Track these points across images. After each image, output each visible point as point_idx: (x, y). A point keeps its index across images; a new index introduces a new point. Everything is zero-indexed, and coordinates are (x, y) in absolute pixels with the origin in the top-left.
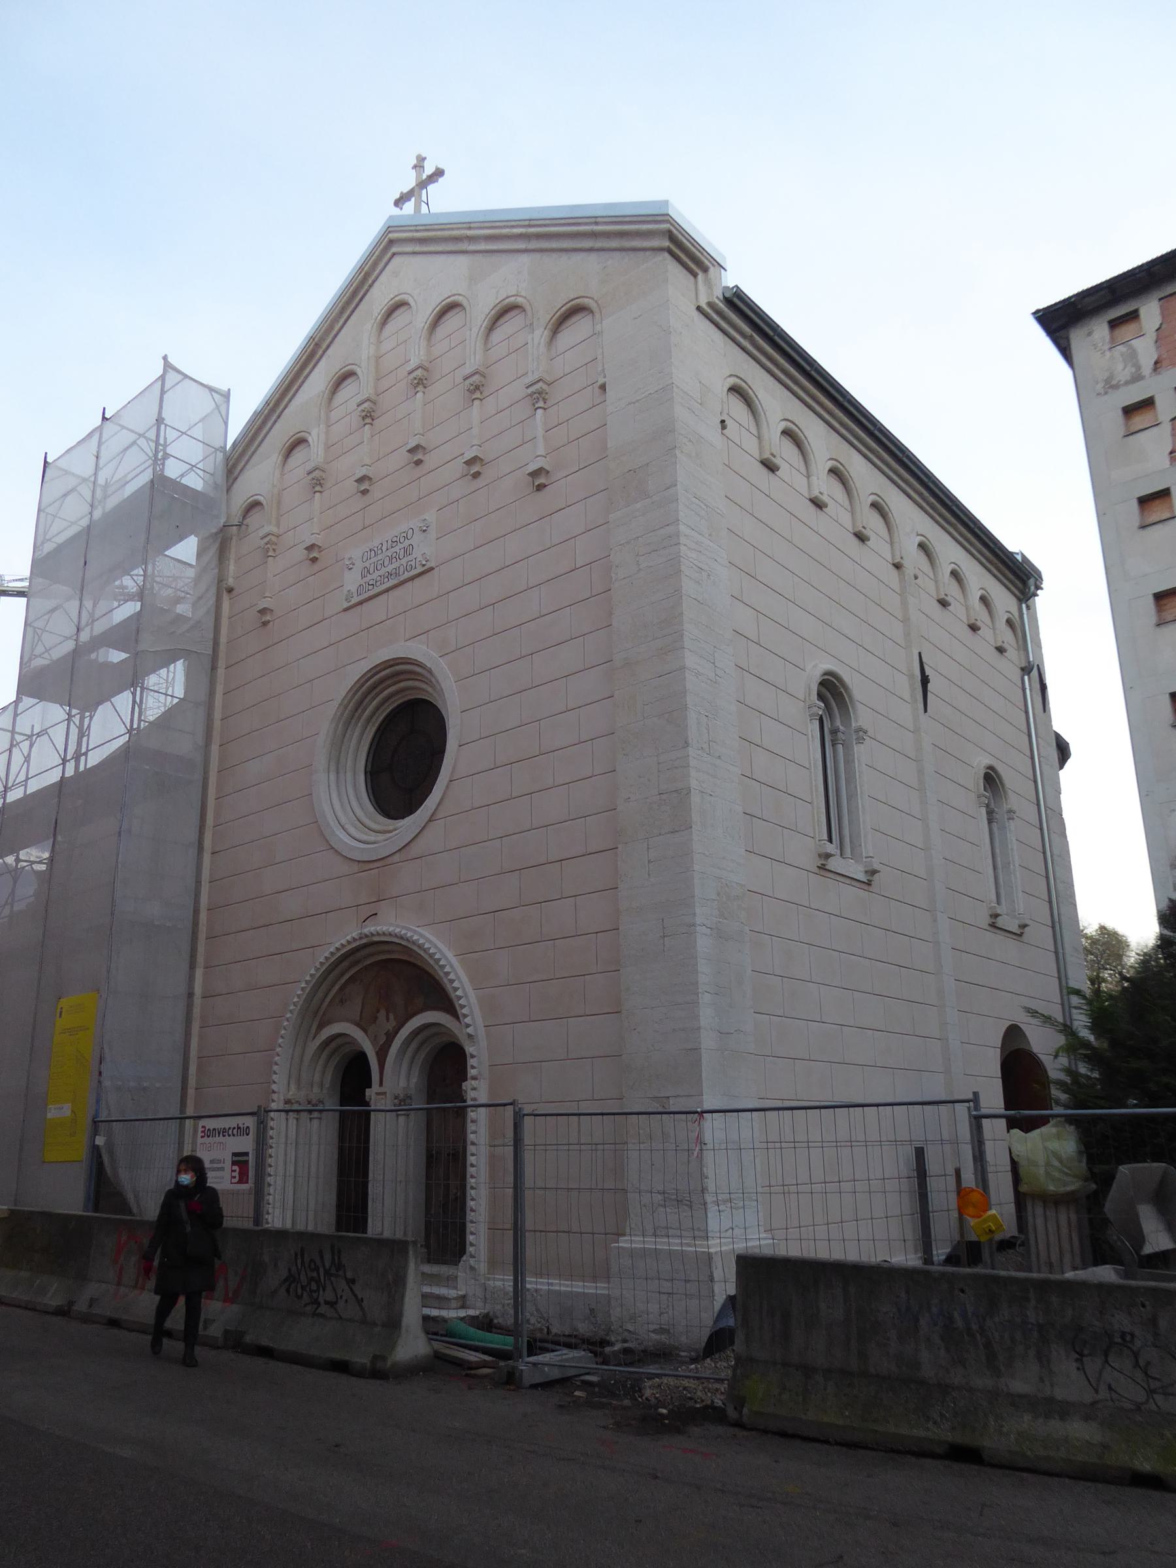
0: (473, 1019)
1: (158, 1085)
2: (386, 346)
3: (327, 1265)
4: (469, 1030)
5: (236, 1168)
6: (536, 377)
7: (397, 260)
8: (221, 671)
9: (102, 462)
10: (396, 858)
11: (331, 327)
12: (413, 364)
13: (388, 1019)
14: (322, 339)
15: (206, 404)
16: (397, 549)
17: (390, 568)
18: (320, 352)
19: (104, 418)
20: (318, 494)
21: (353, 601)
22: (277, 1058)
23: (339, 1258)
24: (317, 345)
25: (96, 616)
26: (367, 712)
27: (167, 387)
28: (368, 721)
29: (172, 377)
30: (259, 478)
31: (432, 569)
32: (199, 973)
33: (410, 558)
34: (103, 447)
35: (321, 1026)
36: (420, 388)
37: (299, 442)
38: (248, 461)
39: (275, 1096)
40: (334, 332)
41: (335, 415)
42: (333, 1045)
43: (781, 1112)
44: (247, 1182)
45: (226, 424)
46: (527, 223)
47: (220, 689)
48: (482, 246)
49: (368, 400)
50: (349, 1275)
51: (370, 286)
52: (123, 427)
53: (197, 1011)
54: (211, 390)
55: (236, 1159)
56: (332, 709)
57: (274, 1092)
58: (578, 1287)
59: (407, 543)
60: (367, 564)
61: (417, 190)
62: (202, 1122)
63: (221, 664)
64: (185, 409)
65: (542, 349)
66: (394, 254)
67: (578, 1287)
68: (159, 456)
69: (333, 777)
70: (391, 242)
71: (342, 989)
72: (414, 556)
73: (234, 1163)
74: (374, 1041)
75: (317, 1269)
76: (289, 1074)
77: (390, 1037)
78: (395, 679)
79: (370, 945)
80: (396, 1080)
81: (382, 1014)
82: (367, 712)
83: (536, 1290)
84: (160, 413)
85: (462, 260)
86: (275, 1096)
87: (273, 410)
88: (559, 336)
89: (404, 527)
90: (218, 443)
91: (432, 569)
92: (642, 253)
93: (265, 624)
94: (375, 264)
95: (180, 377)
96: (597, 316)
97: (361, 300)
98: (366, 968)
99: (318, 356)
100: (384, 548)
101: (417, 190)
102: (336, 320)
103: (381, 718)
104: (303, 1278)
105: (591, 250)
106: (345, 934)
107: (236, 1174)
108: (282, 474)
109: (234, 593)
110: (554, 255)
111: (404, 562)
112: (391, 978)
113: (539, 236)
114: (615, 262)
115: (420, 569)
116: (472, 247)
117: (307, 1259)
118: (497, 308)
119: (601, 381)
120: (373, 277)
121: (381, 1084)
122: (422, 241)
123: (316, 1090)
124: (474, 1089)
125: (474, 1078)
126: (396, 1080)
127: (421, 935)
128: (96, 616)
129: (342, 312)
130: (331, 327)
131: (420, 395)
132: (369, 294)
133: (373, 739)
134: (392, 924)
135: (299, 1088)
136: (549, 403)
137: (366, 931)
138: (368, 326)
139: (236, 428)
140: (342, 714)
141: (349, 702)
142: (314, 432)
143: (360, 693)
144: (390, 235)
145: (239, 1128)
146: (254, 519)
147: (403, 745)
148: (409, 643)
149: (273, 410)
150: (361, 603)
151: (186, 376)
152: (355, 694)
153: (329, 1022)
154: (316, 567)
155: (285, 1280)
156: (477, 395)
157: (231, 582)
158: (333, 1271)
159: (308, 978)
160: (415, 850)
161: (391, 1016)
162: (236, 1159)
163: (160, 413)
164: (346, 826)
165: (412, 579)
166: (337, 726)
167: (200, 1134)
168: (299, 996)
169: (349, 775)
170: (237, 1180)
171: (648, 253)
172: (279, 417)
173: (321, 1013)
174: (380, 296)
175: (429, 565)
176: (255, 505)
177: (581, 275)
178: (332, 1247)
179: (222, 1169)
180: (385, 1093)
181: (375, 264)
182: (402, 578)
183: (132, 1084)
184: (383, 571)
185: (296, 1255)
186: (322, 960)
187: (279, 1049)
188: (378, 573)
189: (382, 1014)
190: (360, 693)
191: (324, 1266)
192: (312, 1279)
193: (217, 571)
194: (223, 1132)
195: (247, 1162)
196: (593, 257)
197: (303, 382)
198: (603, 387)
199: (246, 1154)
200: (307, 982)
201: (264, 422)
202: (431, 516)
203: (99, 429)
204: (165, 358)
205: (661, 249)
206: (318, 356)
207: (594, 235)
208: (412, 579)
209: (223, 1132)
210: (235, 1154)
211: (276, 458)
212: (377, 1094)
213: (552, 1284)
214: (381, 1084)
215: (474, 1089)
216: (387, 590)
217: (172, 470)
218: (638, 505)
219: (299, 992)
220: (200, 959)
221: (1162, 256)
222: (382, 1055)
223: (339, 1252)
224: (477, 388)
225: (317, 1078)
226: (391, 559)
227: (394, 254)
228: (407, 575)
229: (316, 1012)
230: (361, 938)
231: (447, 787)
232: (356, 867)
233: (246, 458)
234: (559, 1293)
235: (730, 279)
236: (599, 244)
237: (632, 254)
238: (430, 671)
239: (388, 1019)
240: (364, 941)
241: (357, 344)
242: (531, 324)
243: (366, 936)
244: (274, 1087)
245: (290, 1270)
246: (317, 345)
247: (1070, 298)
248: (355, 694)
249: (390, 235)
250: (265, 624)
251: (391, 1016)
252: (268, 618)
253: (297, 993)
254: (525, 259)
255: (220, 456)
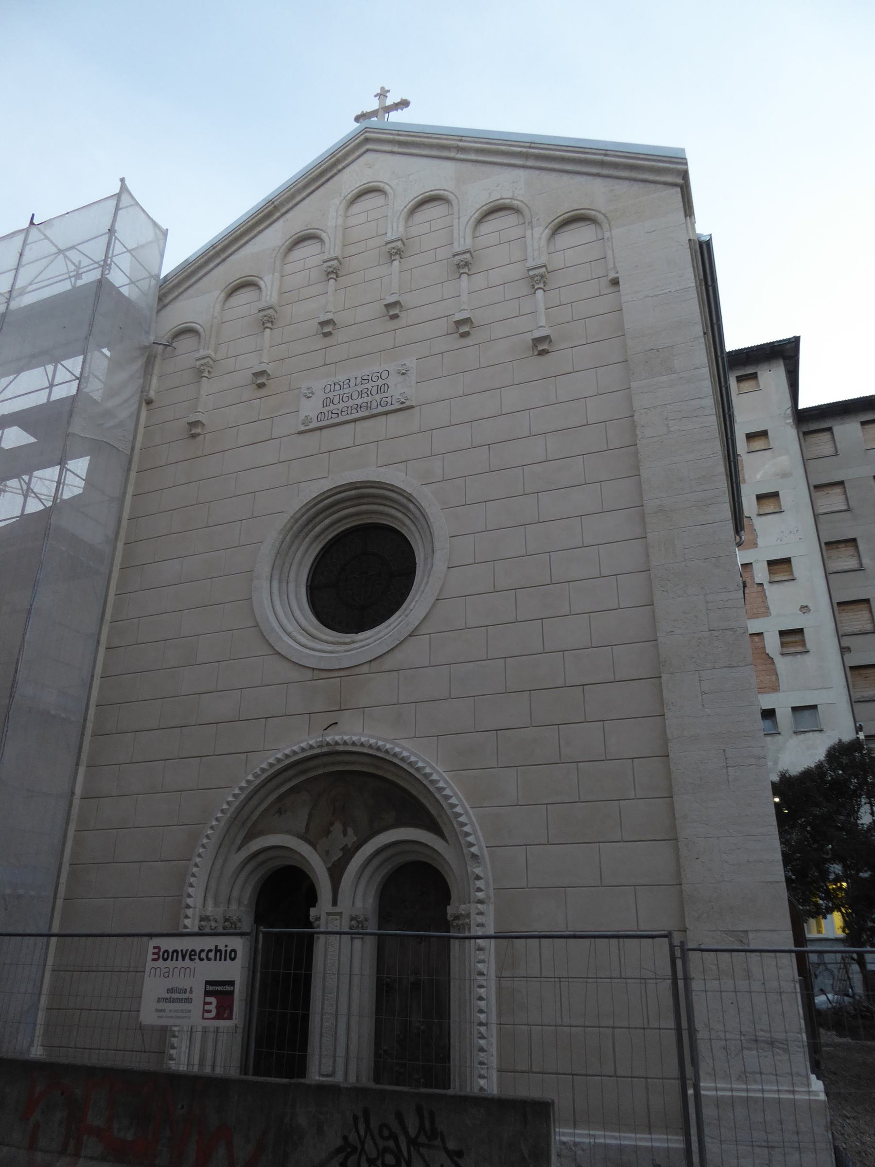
0: (477, 838)
1: (32, 893)
2: (352, 221)
3: (412, 1133)
4: (473, 849)
5: (213, 1000)
6: (539, 262)
7: (369, 156)
8: (133, 474)
9: (25, 259)
10: (365, 669)
11: (293, 196)
12: (390, 236)
13: (345, 833)
14: (282, 204)
15: (149, 234)
16: (369, 386)
17: (359, 401)
18: (278, 214)
19: (32, 223)
20: (268, 330)
21: (311, 426)
22: (195, 870)
23: (432, 1122)
24: (276, 208)
25: (56, 382)
26: (318, 529)
27: (29, 240)
28: (317, 537)
29: (125, 198)
30: (193, 308)
31: (412, 407)
32: (82, 770)
33: (385, 395)
34: (27, 248)
35: (249, 837)
36: (397, 257)
37: (247, 284)
38: (182, 293)
39: (189, 912)
40: (294, 202)
41: (288, 268)
42: (261, 858)
43: (621, 940)
44: (230, 1017)
45: (162, 256)
46: (528, 145)
47: (130, 490)
48: (473, 157)
49: (337, 259)
50: (451, 1145)
51: (339, 171)
52: (47, 238)
53: (75, 811)
54: (155, 224)
55: (210, 988)
56: (283, 520)
57: (188, 907)
58: (629, 1139)
59: (380, 382)
60: (331, 395)
61: (381, 112)
62: (155, 942)
63: (135, 467)
64: (130, 233)
65: (543, 242)
66: (368, 150)
67: (629, 1139)
68: (106, 264)
69: (275, 584)
70: (367, 140)
71: (280, 798)
72: (390, 393)
73: (207, 993)
74: (325, 855)
75: (394, 1137)
76: (211, 890)
77: (348, 854)
78: (356, 502)
79: (332, 753)
80: (347, 903)
81: (338, 827)
82: (318, 529)
83: (576, 1144)
84: (113, 225)
85: (449, 164)
86: (189, 912)
87: (217, 254)
88: (557, 237)
89: (376, 369)
90: (155, 272)
91: (412, 407)
92: (652, 185)
93: (194, 436)
94: (347, 155)
95: (132, 202)
96: (606, 226)
97: (328, 180)
98: (315, 778)
99: (275, 217)
100: (352, 383)
101: (381, 112)
102: (306, 187)
103: (330, 537)
104: (369, 1146)
105: (598, 175)
106: (301, 740)
107: (213, 1007)
108: (223, 310)
109: (152, 406)
110: (554, 174)
111: (378, 397)
112: (362, 791)
113: (537, 157)
114: (622, 188)
115: (397, 406)
116: (460, 156)
117: (374, 1124)
118: (492, 205)
119: (612, 275)
120: (343, 164)
121: (335, 903)
122: (400, 143)
123: (234, 906)
124: (481, 913)
125: (481, 902)
126: (347, 903)
127: (404, 748)
128: (56, 382)
129: (306, 187)
130: (293, 196)
131: (396, 263)
132: (336, 178)
133: (317, 555)
134: (358, 732)
135: (216, 904)
136: (212, 375)
137: (328, 739)
138: (337, 201)
139: (170, 264)
140: (292, 527)
141: (303, 515)
142: (268, 278)
143: (314, 510)
144: (367, 135)
145: (217, 950)
146: (185, 344)
147: (361, 566)
148: (381, 469)
149: (217, 254)
150: (320, 429)
151: (137, 204)
152: (308, 510)
153: (261, 833)
154: (263, 392)
155: (339, 1151)
156: (466, 270)
157: (152, 394)
158: (423, 1139)
159: (243, 784)
160: (389, 663)
161: (350, 831)
162: (210, 988)
163: (113, 225)
164: (295, 634)
165: (386, 413)
166: (284, 538)
167: (150, 956)
168: (228, 803)
169: (292, 586)
170: (213, 1014)
171: (659, 186)
172: (224, 260)
173: (249, 824)
174: (352, 178)
175: (408, 403)
176: (187, 331)
177: (592, 193)
178: (419, 1109)
179: (189, 1000)
180: (340, 914)
181: (347, 155)
182: (374, 412)
183: (8, 891)
184: (350, 403)
185: (356, 1118)
186: (264, 765)
187: (198, 860)
188: (342, 405)
189: (338, 827)
190: (314, 510)
191: (406, 1133)
192: (386, 1150)
193: (142, 380)
194: (192, 955)
195: (232, 992)
196: (598, 180)
197: (255, 236)
198: (615, 282)
199: (232, 983)
200: (242, 789)
201: (206, 263)
202: (411, 363)
203: (27, 231)
204: (122, 180)
205: (675, 185)
206: (275, 217)
207: (602, 164)
208: (386, 413)
209: (192, 955)
210: (208, 983)
211: (218, 294)
212: (328, 914)
213: (594, 1136)
214: (335, 903)
215: (481, 913)
216: (354, 421)
217: (117, 278)
218: (665, 378)
219: (230, 799)
220: (84, 757)
221: (758, 346)
222: (336, 873)
223: (432, 1115)
224: (467, 264)
225: (235, 894)
226: (360, 394)
227: (368, 150)
228: (380, 409)
229: (247, 822)
230: (319, 747)
231: (434, 605)
232: (309, 674)
233: (180, 290)
234: (606, 1146)
235: (703, 227)
236: (605, 171)
237: (642, 185)
238: (409, 498)
239: (345, 833)
240: (325, 749)
241: (325, 210)
242: (531, 222)
243: (328, 744)
244: (189, 901)
245: (345, 1138)
246: (276, 208)
247: (773, 343)
248: (308, 510)
249: (367, 135)
250: (194, 436)
251: (350, 831)
252: (199, 431)
253: (228, 800)
254: (521, 173)
255: (153, 282)
